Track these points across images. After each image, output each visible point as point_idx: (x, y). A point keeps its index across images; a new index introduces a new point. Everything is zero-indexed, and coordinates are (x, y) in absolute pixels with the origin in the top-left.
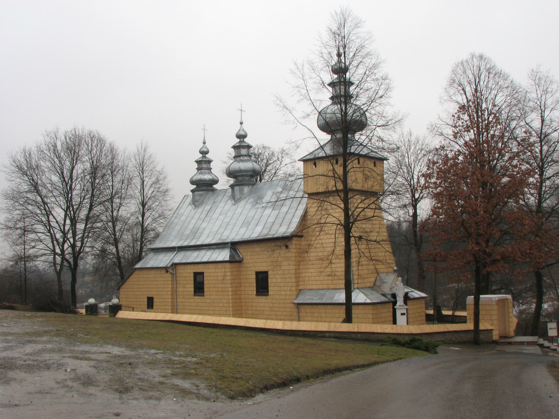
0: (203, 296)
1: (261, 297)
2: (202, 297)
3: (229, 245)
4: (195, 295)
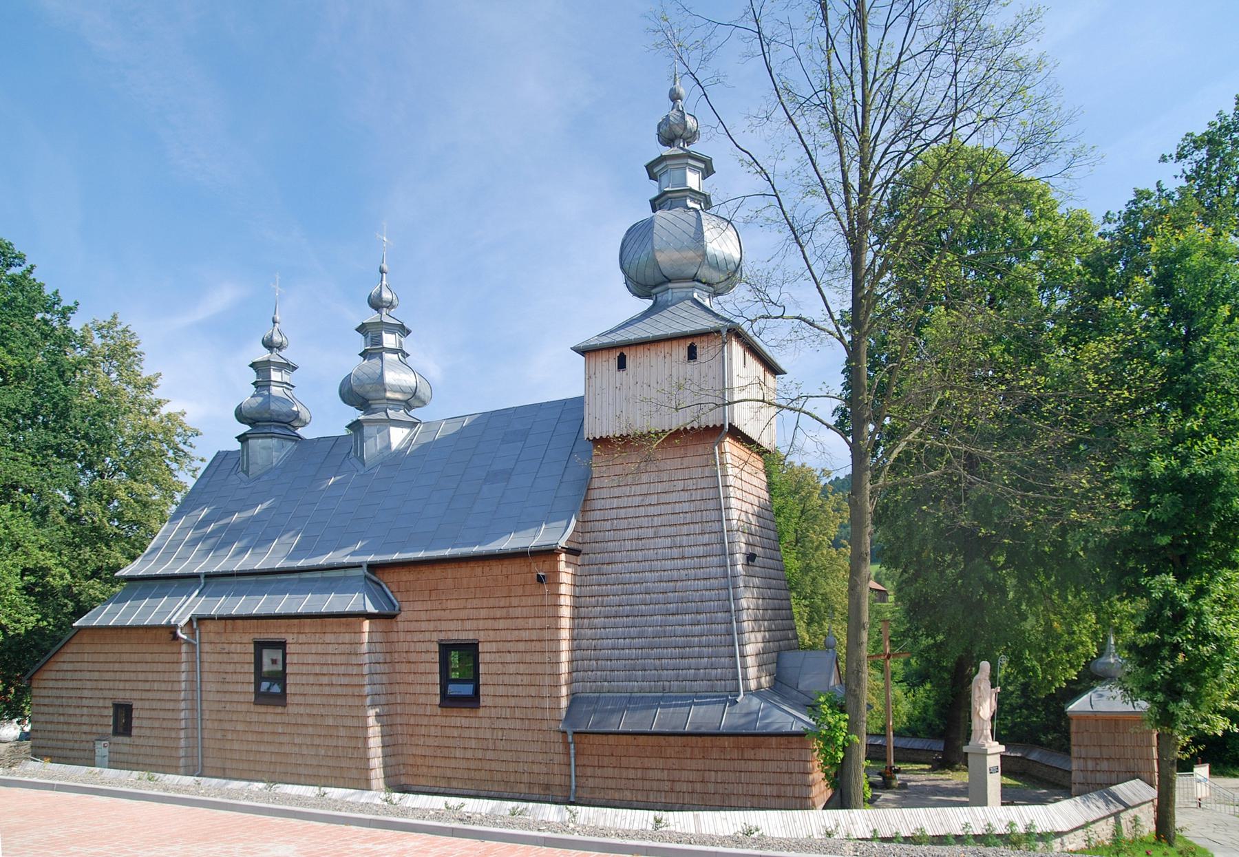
0: (284, 705)
1: (455, 712)
2: (279, 710)
3: (363, 571)
4: (255, 703)
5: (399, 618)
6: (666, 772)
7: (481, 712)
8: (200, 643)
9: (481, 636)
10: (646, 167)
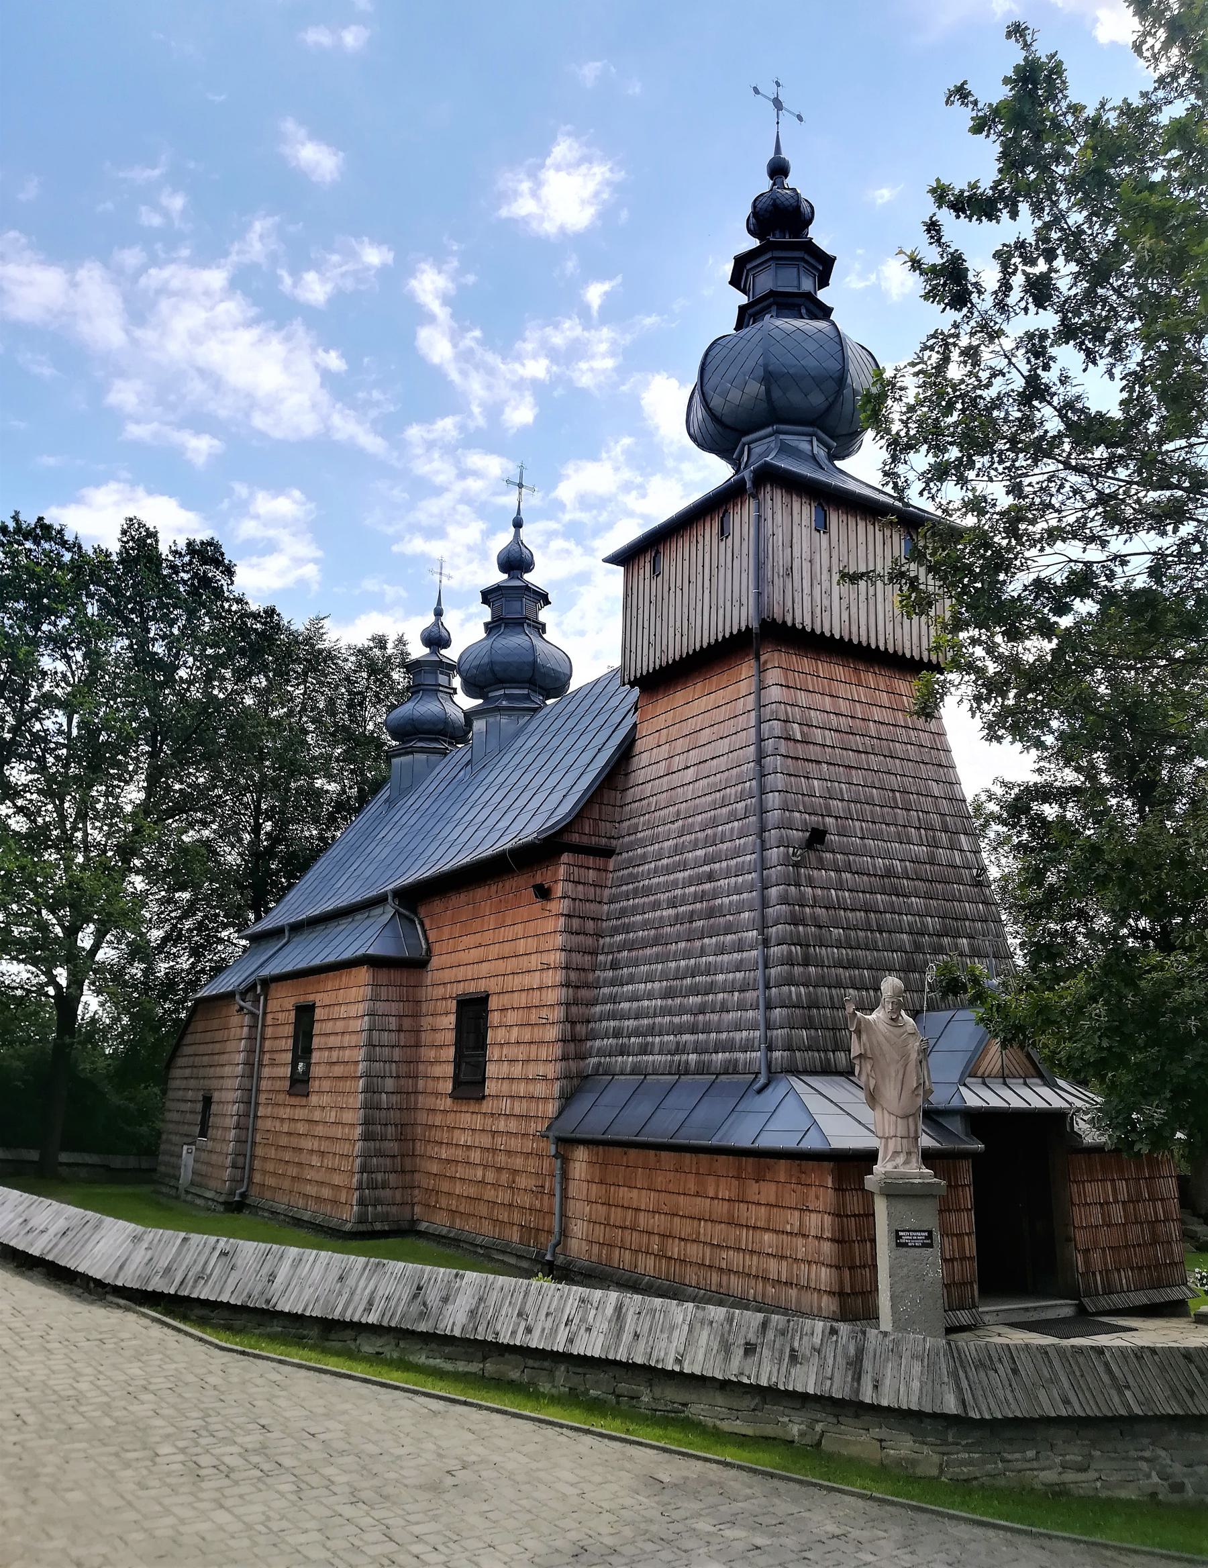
5: (430, 967)
6: (657, 1216)
7: (487, 1106)
8: (265, 1013)
9: (492, 985)
10: (731, 283)
